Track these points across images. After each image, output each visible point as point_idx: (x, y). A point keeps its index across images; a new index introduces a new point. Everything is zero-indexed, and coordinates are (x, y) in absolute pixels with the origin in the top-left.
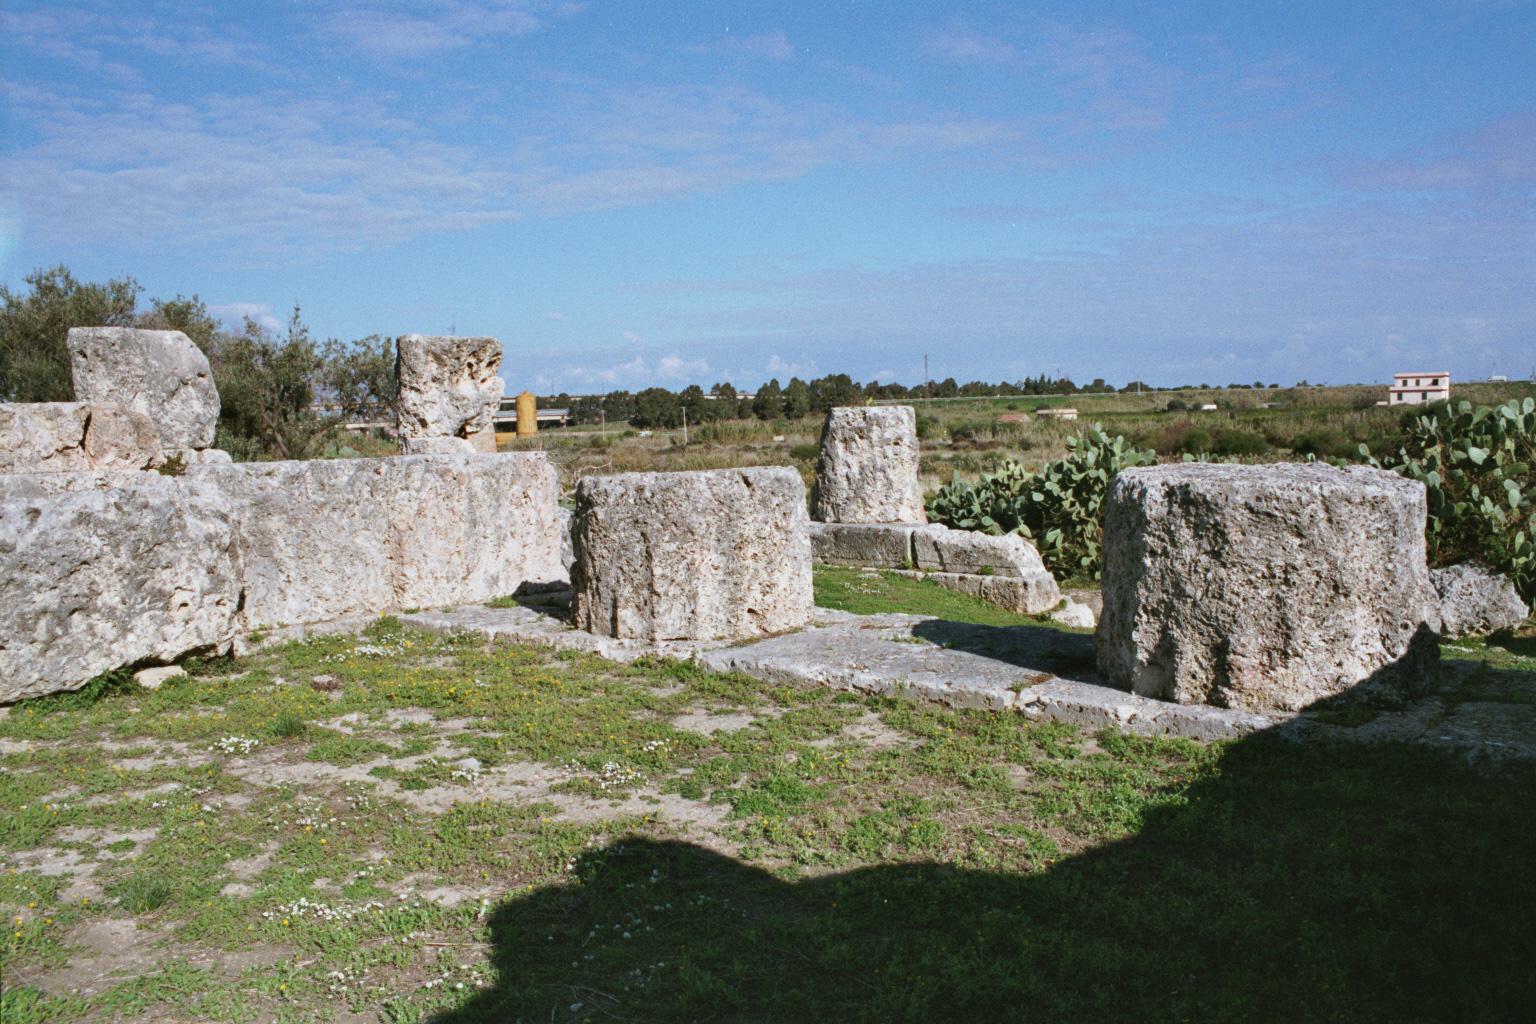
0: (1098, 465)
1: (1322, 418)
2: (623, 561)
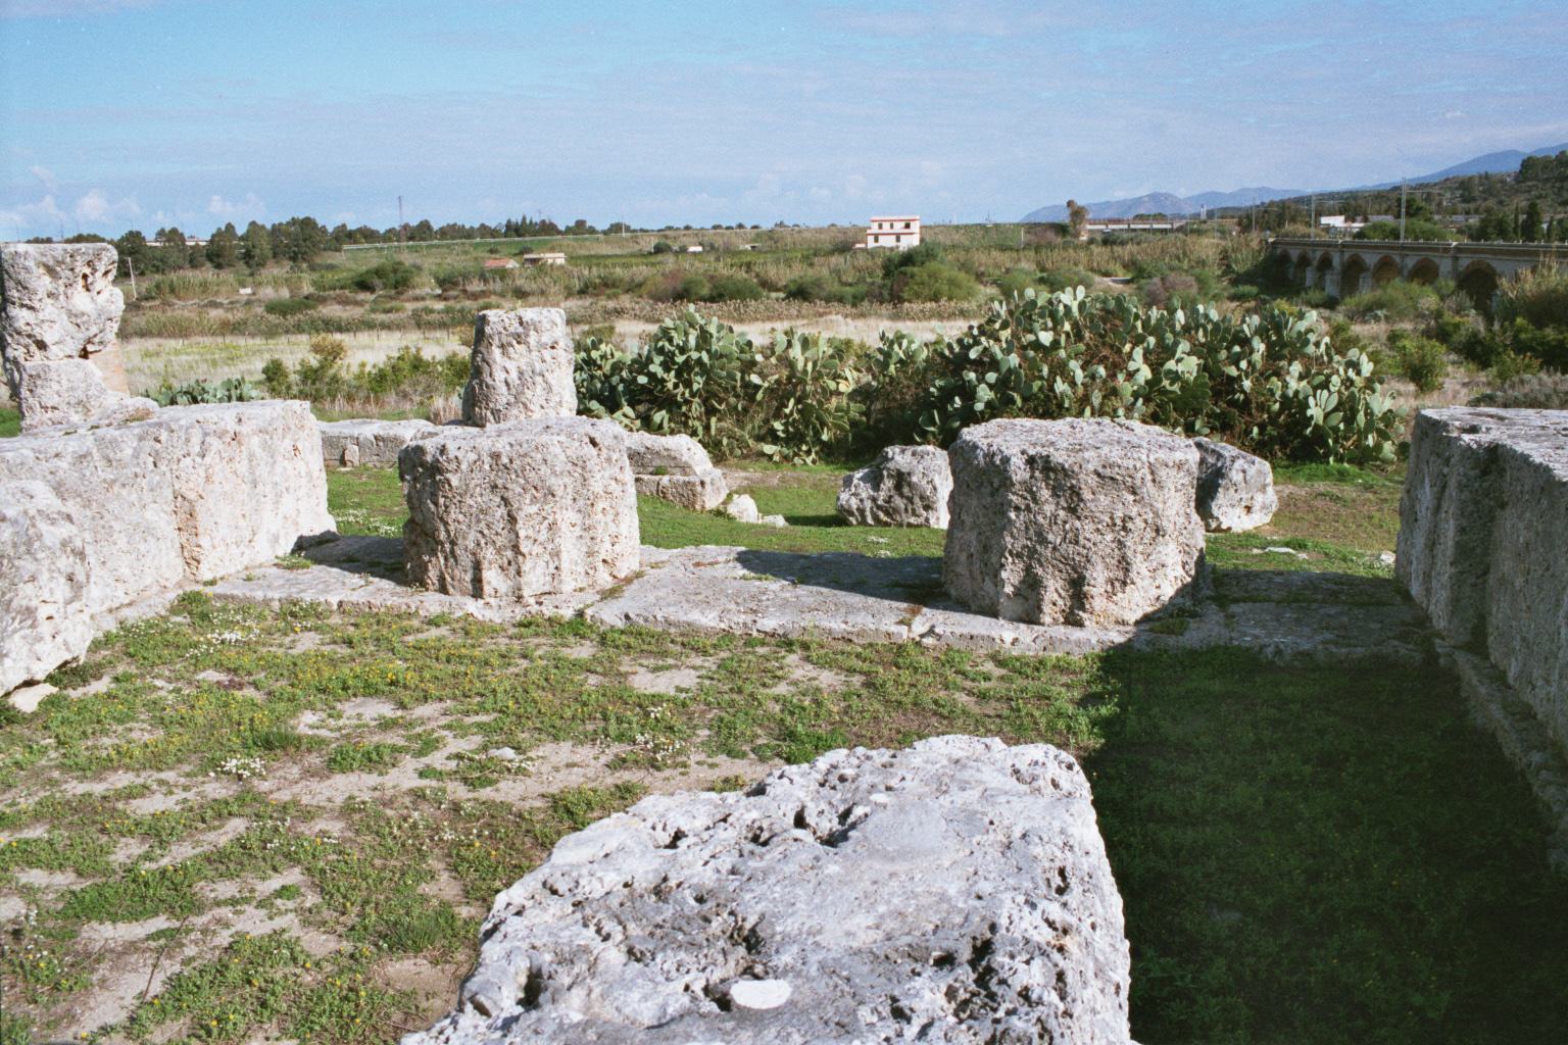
0: (698, 348)
1: (808, 260)
2: (482, 525)
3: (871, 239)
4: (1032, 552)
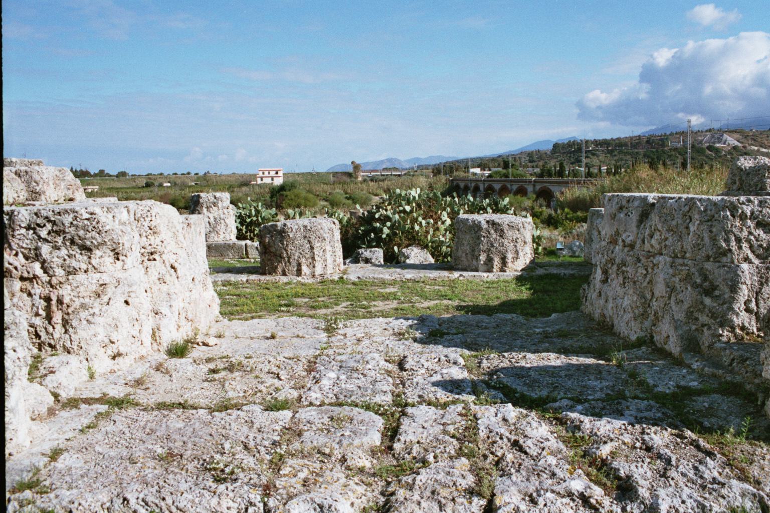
2: (301, 251)
3: (259, 180)
4: (489, 250)
